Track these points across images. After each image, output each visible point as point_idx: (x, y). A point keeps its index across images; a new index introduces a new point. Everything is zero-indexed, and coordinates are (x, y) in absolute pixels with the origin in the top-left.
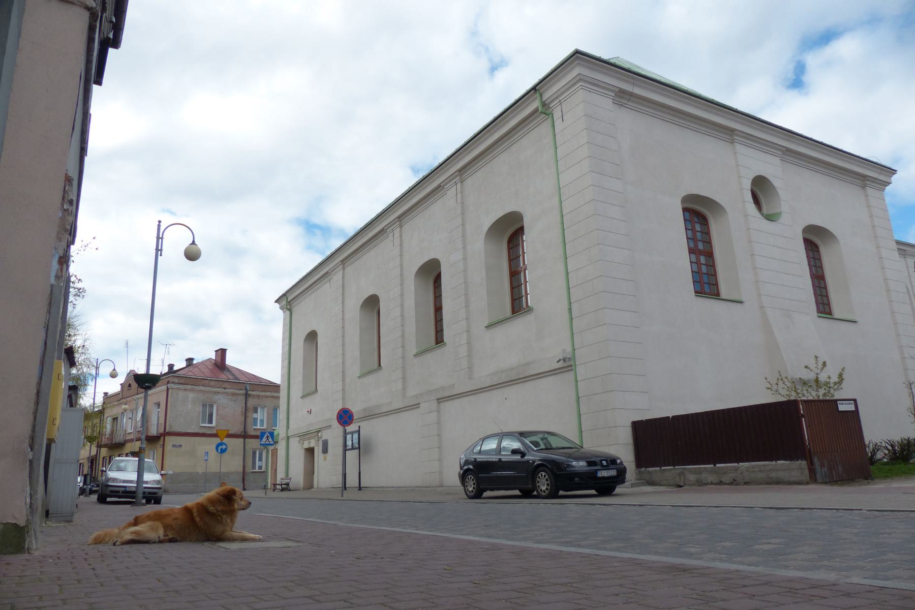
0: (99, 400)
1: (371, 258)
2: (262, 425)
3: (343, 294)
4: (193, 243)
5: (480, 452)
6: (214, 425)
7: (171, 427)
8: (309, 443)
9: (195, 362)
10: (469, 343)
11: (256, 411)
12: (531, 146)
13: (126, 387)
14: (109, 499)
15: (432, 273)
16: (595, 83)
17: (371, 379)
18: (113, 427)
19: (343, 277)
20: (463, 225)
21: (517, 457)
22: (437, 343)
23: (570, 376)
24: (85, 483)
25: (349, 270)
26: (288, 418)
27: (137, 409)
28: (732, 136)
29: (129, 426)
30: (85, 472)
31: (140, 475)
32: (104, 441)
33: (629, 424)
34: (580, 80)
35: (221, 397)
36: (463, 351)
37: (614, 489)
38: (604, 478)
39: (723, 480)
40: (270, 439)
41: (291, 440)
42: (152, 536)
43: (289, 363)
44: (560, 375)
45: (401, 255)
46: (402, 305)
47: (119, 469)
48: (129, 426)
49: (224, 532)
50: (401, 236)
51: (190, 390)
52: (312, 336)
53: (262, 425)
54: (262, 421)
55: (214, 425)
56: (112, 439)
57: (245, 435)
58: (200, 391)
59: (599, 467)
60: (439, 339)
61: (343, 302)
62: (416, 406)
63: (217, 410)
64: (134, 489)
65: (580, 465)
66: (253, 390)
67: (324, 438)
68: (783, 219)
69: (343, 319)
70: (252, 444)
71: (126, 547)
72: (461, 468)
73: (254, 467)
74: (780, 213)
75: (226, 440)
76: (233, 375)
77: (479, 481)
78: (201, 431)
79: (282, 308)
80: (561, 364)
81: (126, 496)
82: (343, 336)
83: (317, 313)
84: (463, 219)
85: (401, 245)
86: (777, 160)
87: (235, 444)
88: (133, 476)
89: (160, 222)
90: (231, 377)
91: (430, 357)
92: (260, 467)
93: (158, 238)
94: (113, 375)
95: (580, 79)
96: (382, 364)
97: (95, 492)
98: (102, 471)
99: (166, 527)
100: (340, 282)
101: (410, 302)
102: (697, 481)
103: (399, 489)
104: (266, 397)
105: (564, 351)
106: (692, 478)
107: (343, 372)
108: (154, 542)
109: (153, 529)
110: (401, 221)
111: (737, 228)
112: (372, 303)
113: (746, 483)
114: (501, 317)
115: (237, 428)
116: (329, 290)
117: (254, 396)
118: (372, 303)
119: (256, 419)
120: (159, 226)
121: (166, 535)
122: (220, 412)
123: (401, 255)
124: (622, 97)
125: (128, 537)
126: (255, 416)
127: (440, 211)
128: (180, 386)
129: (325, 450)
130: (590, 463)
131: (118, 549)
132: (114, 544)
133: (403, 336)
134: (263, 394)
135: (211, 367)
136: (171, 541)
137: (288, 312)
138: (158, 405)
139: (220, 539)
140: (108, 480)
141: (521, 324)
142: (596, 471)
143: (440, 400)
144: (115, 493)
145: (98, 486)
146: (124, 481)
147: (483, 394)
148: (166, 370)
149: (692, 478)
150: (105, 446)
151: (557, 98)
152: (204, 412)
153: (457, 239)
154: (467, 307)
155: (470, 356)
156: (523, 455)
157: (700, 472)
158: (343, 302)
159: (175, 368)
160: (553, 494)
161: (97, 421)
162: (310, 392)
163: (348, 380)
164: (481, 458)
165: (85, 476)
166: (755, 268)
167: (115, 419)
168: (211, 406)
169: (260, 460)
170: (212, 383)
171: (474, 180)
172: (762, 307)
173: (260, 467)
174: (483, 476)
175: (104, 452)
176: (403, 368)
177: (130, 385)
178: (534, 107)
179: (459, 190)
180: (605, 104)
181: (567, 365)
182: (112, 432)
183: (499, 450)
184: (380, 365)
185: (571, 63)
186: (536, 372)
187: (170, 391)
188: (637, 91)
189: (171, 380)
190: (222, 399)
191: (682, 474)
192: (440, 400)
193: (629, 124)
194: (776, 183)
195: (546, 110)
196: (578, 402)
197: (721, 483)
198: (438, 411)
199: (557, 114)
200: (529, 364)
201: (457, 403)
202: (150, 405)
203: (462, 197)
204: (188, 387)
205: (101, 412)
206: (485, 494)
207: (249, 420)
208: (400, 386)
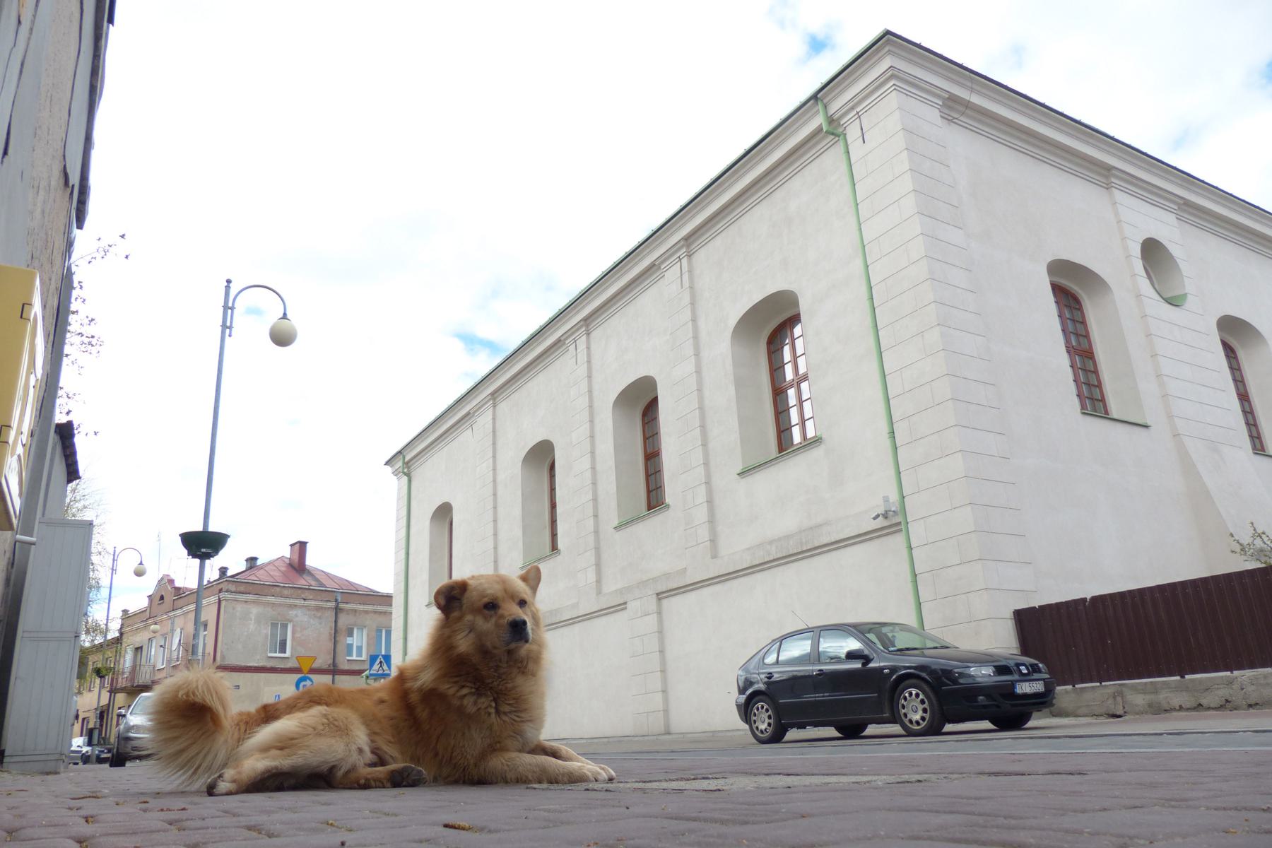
0: (114, 627)
1: (538, 385)
2: (359, 654)
3: (494, 444)
4: (285, 316)
6: (288, 654)
7: (223, 657)
9: (259, 562)
10: (710, 502)
11: (350, 634)
12: (813, 188)
15: (643, 404)
16: (914, 83)
19: (494, 419)
21: (857, 665)
22: (650, 508)
23: (898, 541)
24: (90, 744)
25: (503, 407)
26: (405, 639)
27: (173, 631)
28: (1107, 177)
30: (91, 725)
32: (122, 683)
33: (1009, 614)
34: (892, 77)
35: (299, 612)
36: (701, 514)
37: (1026, 717)
38: (1025, 696)
39: (1204, 702)
40: (385, 667)
43: (408, 554)
44: (868, 543)
45: (590, 377)
46: (593, 453)
50: (588, 348)
51: (254, 602)
52: (444, 513)
53: (359, 654)
54: (360, 648)
55: (288, 654)
56: (133, 679)
58: (269, 604)
59: (1016, 677)
60: (654, 498)
61: (494, 457)
62: (622, 606)
63: (293, 632)
65: (983, 674)
68: (1191, 303)
69: (494, 481)
72: (742, 691)
76: (317, 580)
78: (269, 664)
79: (395, 473)
80: (881, 522)
82: (495, 508)
83: (456, 476)
85: (589, 362)
86: (1171, 218)
89: (229, 281)
90: (313, 583)
91: (641, 529)
93: (226, 307)
94: (139, 573)
96: (560, 545)
98: (119, 715)
100: (490, 426)
101: (606, 446)
102: (1150, 705)
103: (622, 739)
104: (367, 612)
105: (886, 499)
106: (1139, 700)
110: (587, 326)
111: (1127, 311)
113: (1250, 706)
115: (323, 661)
116: (471, 440)
117: (348, 611)
118: (542, 457)
119: (350, 646)
120: (228, 288)
122: (298, 635)
123: (590, 377)
124: (953, 108)
126: (349, 640)
127: (656, 304)
130: (1001, 670)
133: (595, 500)
134: (361, 607)
137: (405, 478)
139: (481, 781)
141: (794, 470)
143: (660, 596)
145: (109, 751)
147: (758, 576)
149: (1139, 700)
150: (122, 690)
151: (852, 108)
152: (273, 635)
153: (686, 345)
154: (705, 445)
155: (712, 521)
157: (1155, 690)
158: (494, 457)
159: (229, 573)
160: (934, 729)
161: (109, 654)
164: (779, 674)
165: (90, 733)
166: (1159, 376)
167: (139, 649)
168: (285, 627)
170: (286, 592)
171: (708, 254)
174: (794, 704)
175: (120, 698)
176: (597, 549)
177: (162, 598)
178: (817, 125)
180: (930, 114)
181: (892, 523)
182: (134, 668)
183: (815, 656)
184: (554, 547)
185: (878, 51)
187: (223, 603)
188: (976, 99)
190: (300, 616)
192: (660, 596)
193: (965, 149)
194: (1174, 250)
195: (834, 130)
198: (659, 613)
199: (853, 133)
200: (819, 526)
201: (692, 597)
204: (251, 597)
205: (118, 641)
206: (792, 734)
207: (341, 648)
208: (591, 576)
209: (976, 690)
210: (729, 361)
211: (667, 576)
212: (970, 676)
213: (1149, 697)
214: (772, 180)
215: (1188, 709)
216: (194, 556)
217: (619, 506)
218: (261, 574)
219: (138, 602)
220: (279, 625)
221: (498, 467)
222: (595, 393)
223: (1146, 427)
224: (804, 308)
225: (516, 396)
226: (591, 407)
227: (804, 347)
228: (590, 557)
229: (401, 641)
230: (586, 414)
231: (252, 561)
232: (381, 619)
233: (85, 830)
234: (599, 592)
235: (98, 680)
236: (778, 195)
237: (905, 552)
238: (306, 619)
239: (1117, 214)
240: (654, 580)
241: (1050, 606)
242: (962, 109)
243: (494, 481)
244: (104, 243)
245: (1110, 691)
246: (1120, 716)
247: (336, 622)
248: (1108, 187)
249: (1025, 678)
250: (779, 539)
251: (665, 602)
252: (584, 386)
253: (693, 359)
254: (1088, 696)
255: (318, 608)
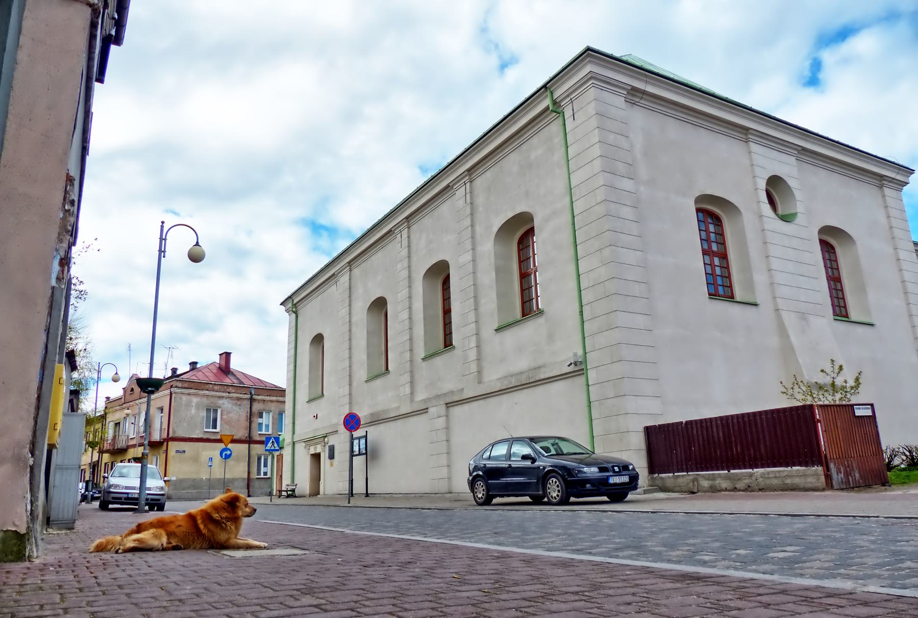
0: (101, 405)
1: (378, 258)
2: (267, 429)
3: (350, 296)
4: (197, 244)
5: (489, 458)
6: (218, 430)
7: (174, 432)
8: (316, 449)
9: (198, 366)
11: (261, 416)
13: (129, 392)
14: (111, 506)
15: (440, 274)
17: (378, 382)
18: (115, 432)
19: (350, 279)
20: (472, 226)
21: (528, 463)
23: (581, 380)
25: (356, 272)
26: (294, 423)
27: (139, 414)
28: (746, 134)
29: (132, 431)
31: (143, 478)
32: (106, 446)
33: (641, 429)
34: (591, 78)
36: (473, 355)
38: (615, 484)
39: (737, 486)
40: (276, 445)
41: (297, 445)
42: (155, 543)
45: (409, 257)
46: (410, 308)
47: (122, 476)
48: (132, 431)
49: (228, 539)
50: (409, 237)
52: (318, 339)
53: (267, 429)
54: (267, 426)
55: (218, 430)
56: (114, 445)
57: (249, 441)
58: (204, 395)
59: (611, 474)
61: (350, 305)
63: (222, 415)
64: (136, 496)
65: (591, 471)
66: (259, 394)
67: (330, 444)
68: (800, 219)
69: (350, 321)
70: (258, 449)
71: (129, 555)
73: (259, 473)
74: (796, 214)
75: (230, 446)
76: (238, 379)
77: (488, 488)
79: (287, 311)
80: (572, 368)
81: (129, 503)
82: (350, 339)
84: (472, 220)
85: (409, 246)
87: (240, 449)
88: (137, 483)
89: (163, 222)
90: (235, 381)
91: (438, 361)
92: (265, 474)
93: (161, 239)
94: (115, 380)
95: (592, 76)
97: (97, 498)
98: (104, 477)
99: (170, 535)
100: (347, 284)
101: (418, 305)
102: (711, 487)
104: (272, 401)
105: (575, 355)
107: (350, 376)
108: (158, 550)
109: (156, 536)
112: (379, 305)
113: (760, 490)
114: (511, 320)
115: (241, 434)
117: (259, 401)
118: (379, 305)
119: (260, 424)
120: (162, 227)
121: (169, 543)
122: (225, 417)
123: (409, 257)
125: (130, 544)
126: (260, 420)
128: (183, 391)
129: (332, 456)
130: (602, 470)
131: (119, 557)
132: (117, 552)
133: (411, 339)
134: (268, 398)
135: (215, 371)
136: (176, 548)
137: (294, 315)
138: (162, 409)
140: (110, 486)
142: (608, 477)
143: (448, 405)
144: (117, 500)
145: (100, 492)
146: (127, 488)
147: (505, 396)
148: (169, 374)
149: (705, 484)
151: (568, 96)
152: (208, 417)
153: (465, 241)
156: (534, 460)
158: (350, 305)
159: (178, 372)
160: (564, 501)
161: (98, 426)
162: (316, 397)
163: (354, 384)
165: (87, 482)
166: (770, 270)
168: (216, 411)
169: (265, 466)
170: (216, 388)
172: (777, 310)
173: (265, 474)
174: (492, 482)
175: (106, 457)
176: (412, 372)
177: (132, 390)
178: (544, 106)
179: (468, 190)
181: (579, 369)
182: (114, 438)
183: (509, 456)
185: (583, 60)
186: (552, 375)
187: (173, 395)
188: (650, 89)
189: (174, 384)
190: (226, 404)
191: (695, 480)
193: (640, 120)
194: (792, 183)
195: (557, 108)
196: (590, 406)
197: (735, 489)
198: (447, 416)
199: (568, 113)
200: (540, 367)
201: (466, 407)
202: (153, 410)
203: (471, 198)
204: (192, 391)
205: (103, 417)
206: (495, 501)
207: (255, 426)
208: (407, 390)
209: (588, 481)
210: (492, 256)
211: (452, 393)
212: (583, 472)
213: (710, 482)
214: (520, 137)
215: (729, 491)
216: (144, 392)
217: (425, 344)
218: (200, 375)
219: (116, 391)
220: (212, 411)
221: (353, 312)
222: (413, 268)
223: (756, 305)
224: (537, 223)
225: (364, 265)
226: (409, 277)
227: (542, 246)
228: (406, 378)
229: (291, 425)
230: (406, 283)
231: (193, 364)
232: (281, 406)
233: (88, 565)
234: (412, 400)
235: (90, 449)
236: (524, 147)
237: (585, 387)
238: (230, 406)
239: (751, 159)
240: (445, 394)
241: (664, 425)
242: (641, 95)
243: (350, 321)
244: (86, 244)
245: (691, 478)
246: (694, 493)
247: (251, 408)
248: (747, 141)
249: (618, 474)
250: (517, 374)
251: (451, 409)
252: (406, 264)
253: (471, 252)
254: (680, 480)
255: (239, 399)
